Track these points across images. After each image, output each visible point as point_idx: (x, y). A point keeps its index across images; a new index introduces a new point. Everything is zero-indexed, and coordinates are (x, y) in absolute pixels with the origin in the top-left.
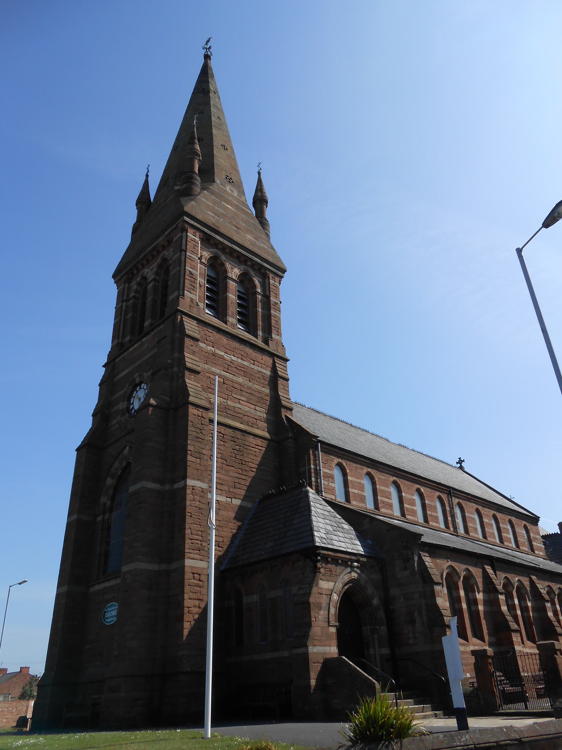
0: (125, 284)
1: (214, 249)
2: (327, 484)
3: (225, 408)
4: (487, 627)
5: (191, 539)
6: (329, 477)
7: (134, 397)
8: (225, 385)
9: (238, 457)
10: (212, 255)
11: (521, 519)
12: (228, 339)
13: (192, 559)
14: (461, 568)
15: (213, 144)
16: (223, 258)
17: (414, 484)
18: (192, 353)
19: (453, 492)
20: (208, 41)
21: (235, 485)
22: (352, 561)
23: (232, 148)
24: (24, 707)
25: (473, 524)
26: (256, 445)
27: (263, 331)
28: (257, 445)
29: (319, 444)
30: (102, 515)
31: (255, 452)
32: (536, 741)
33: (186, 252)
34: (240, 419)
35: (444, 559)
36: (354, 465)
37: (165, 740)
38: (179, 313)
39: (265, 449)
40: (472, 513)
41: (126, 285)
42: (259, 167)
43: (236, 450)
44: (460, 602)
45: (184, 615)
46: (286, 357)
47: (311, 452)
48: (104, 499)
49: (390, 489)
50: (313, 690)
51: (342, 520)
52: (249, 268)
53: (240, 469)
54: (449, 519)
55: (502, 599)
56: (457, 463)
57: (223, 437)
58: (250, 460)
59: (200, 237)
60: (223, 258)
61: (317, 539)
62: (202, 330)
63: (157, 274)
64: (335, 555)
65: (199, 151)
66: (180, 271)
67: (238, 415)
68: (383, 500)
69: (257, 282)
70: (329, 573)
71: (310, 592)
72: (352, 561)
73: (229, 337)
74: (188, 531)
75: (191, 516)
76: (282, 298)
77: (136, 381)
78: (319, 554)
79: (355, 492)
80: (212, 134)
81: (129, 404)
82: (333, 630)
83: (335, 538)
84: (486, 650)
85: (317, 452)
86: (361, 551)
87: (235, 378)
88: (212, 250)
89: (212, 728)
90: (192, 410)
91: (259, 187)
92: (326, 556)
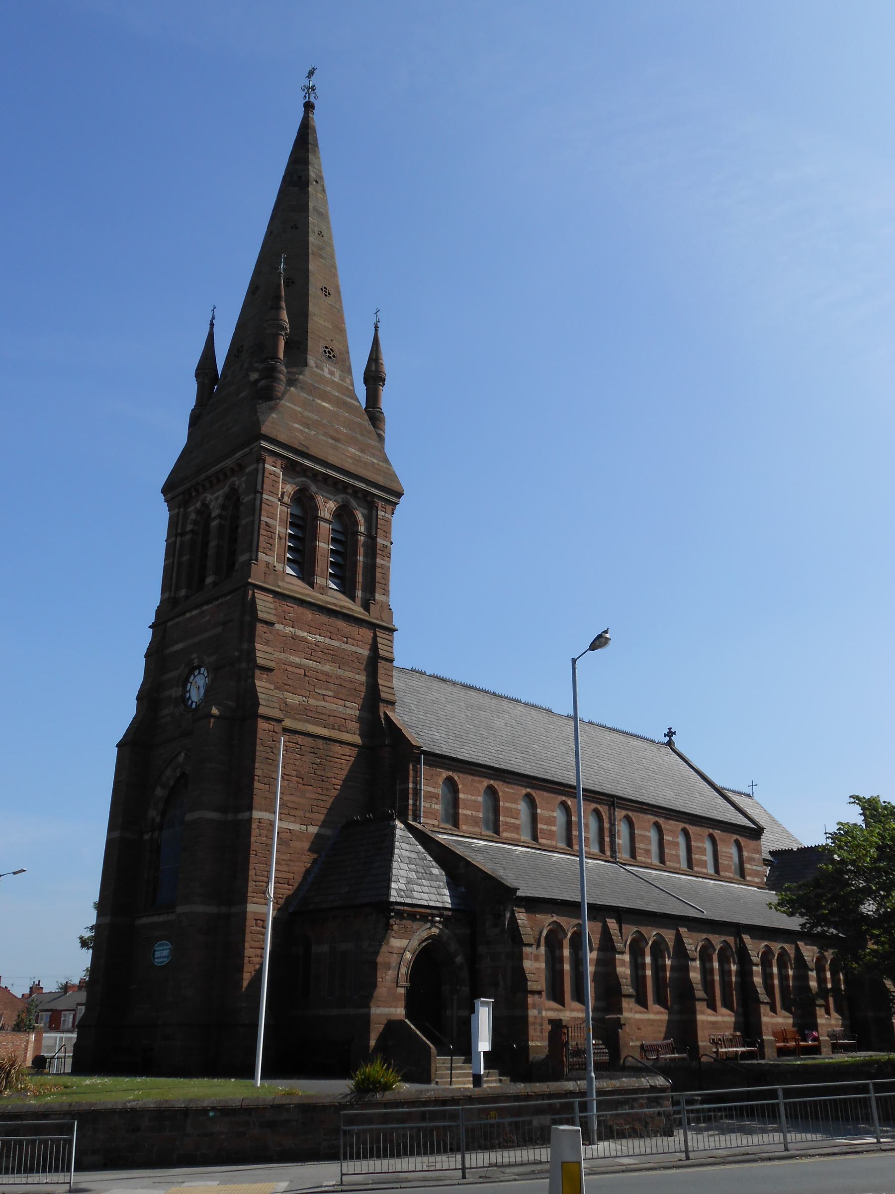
1: (301, 477)
2: (429, 806)
3: (306, 709)
6: (433, 797)
7: (191, 683)
8: (307, 678)
13: (256, 904)
15: (308, 293)
16: (313, 488)
21: (313, 809)
22: (433, 916)
23: (338, 292)
24: (23, 1042)
25: (645, 844)
26: (342, 755)
29: (423, 756)
30: (150, 833)
31: (341, 764)
32: (483, 1097)
33: (262, 493)
34: (324, 722)
36: (470, 778)
37: (220, 1086)
38: (251, 587)
39: (354, 758)
41: (182, 510)
42: (377, 316)
43: (316, 764)
45: (244, 965)
46: (392, 626)
47: (411, 767)
49: (519, 806)
50: (372, 1051)
52: (348, 497)
54: (607, 839)
56: (666, 735)
57: (300, 749)
58: (333, 775)
59: (282, 467)
60: (313, 488)
61: (393, 893)
62: (280, 606)
63: (223, 507)
64: (413, 910)
65: (286, 322)
66: (253, 522)
67: (321, 717)
69: (360, 517)
71: (379, 952)
72: (433, 916)
73: (315, 609)
74: (252, 873)
75: (256, 855)
76: (394, 536)
77: (194, 663)
78: (393, 910)
80: (309, 272)
81: (185, 691)
82: (402, 991)
83: (416, 888)
85: (418, 766)
86: (447, 902)
87: (320, 667)
88: (298, 480)
89: (264, 1081)
90: (262, 725)
91: (374, 354)
92: (402, 912)
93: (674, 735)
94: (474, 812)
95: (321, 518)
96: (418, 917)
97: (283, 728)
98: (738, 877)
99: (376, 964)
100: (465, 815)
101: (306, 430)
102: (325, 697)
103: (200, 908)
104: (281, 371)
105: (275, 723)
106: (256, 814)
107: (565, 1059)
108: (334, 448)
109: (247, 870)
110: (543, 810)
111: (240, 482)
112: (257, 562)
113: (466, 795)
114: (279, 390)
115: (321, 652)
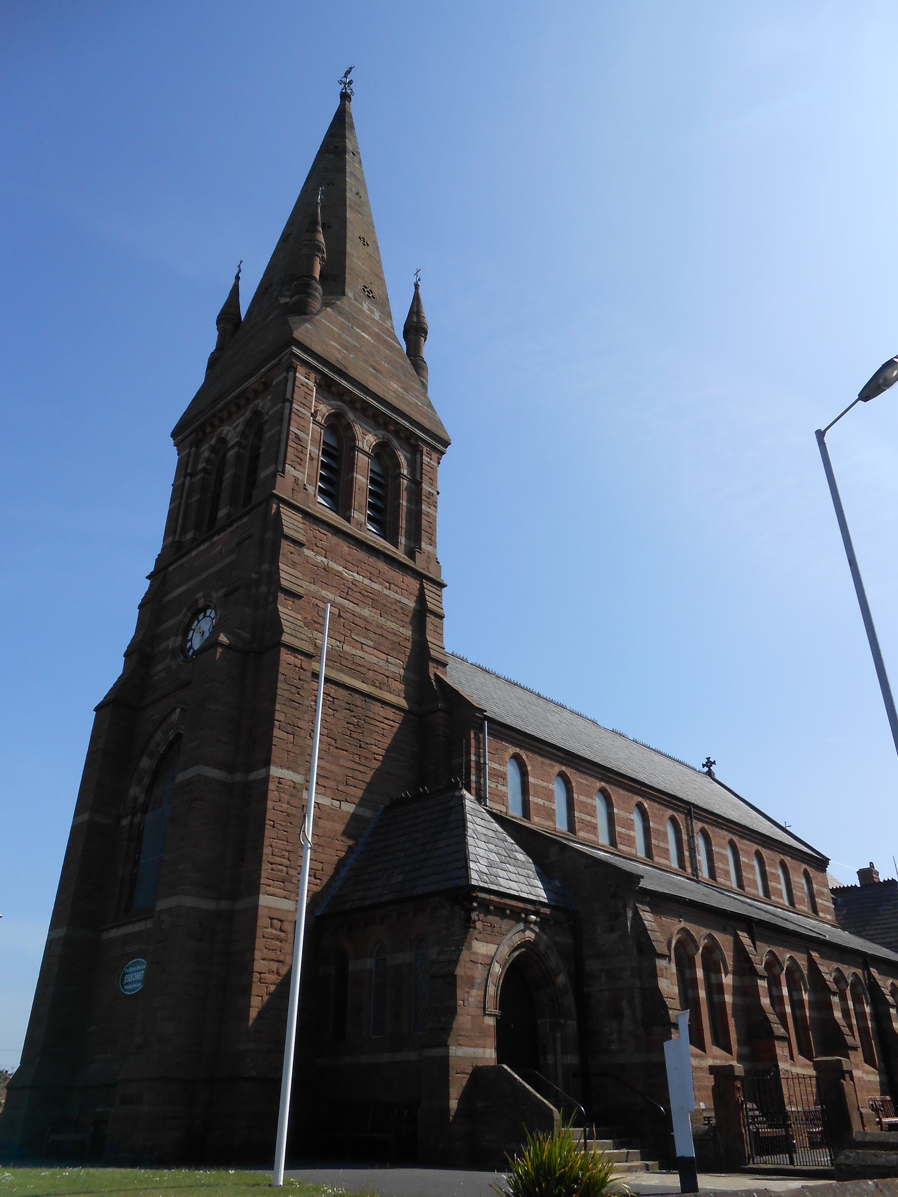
1: (336, 401)
3: (340, 656)
5: (272, 864)
8: (342, 619)
9: (355, 736)
10: (333, 410)
11: (797, 860)
12: (351, 546)
13: (271, 895)
16: (351, 416)
20: (348, 72)
25: (724, 864)
26: (384, 718)
27: (408, 537)
28: (387, 719)
29: (486, 722)
30: (130, 817)
31: (383, 729)
33: (291, 403)
34: (362, 675)
36: (540, 759)
38: (275, 500)
39: (398, 725)
42: (417, 276)
43: (352, 724)
45: (253, 984)
46: (440, 581)
47: (472, 735)
49: (594, 801)
50: (454, 1117)
51: (516, 846)
52: (390, 435)
54: (687, 853)
56: (704, 766)
57: (333, 702)
58: (373, 741)
59: (315, 381)
60: (351, 416)
61: (474, 875)
64: (502, 901)
65: (322, 243)
66: (279, 433)
67: (359, 668)
69: (402, 459)
72: (528, 912)
74: (267, 850)
75: (273, 827)
77: (198, 605)
78: (475, 899)
81: (185, 639)
82: (490, 1021)
84: (733, 1066)
85: (481, 736)
86: (542, 897)
87: (358, 609)
89: (290, 1171)
90: (286, 657)
93: (713, 765)
94: (547, 802)
95: (359, 448)
96: (508, 912)
97: (313, 672)
98: (811, 912)
99: (454, 977)
100: (536, 803)
101: (345, 351)
102: (364, 646)
103: (189, 901)
104: (316, 289)
105: (302, 658)
106: (275, 771)
107: (744, 1131)
108: (376, 378)
109: (261, 846)
110: (620, 809)
111: (263, 403)
112: (284, 475)
113: (536, 779)
114: (314, 306)
115: (360, 593)
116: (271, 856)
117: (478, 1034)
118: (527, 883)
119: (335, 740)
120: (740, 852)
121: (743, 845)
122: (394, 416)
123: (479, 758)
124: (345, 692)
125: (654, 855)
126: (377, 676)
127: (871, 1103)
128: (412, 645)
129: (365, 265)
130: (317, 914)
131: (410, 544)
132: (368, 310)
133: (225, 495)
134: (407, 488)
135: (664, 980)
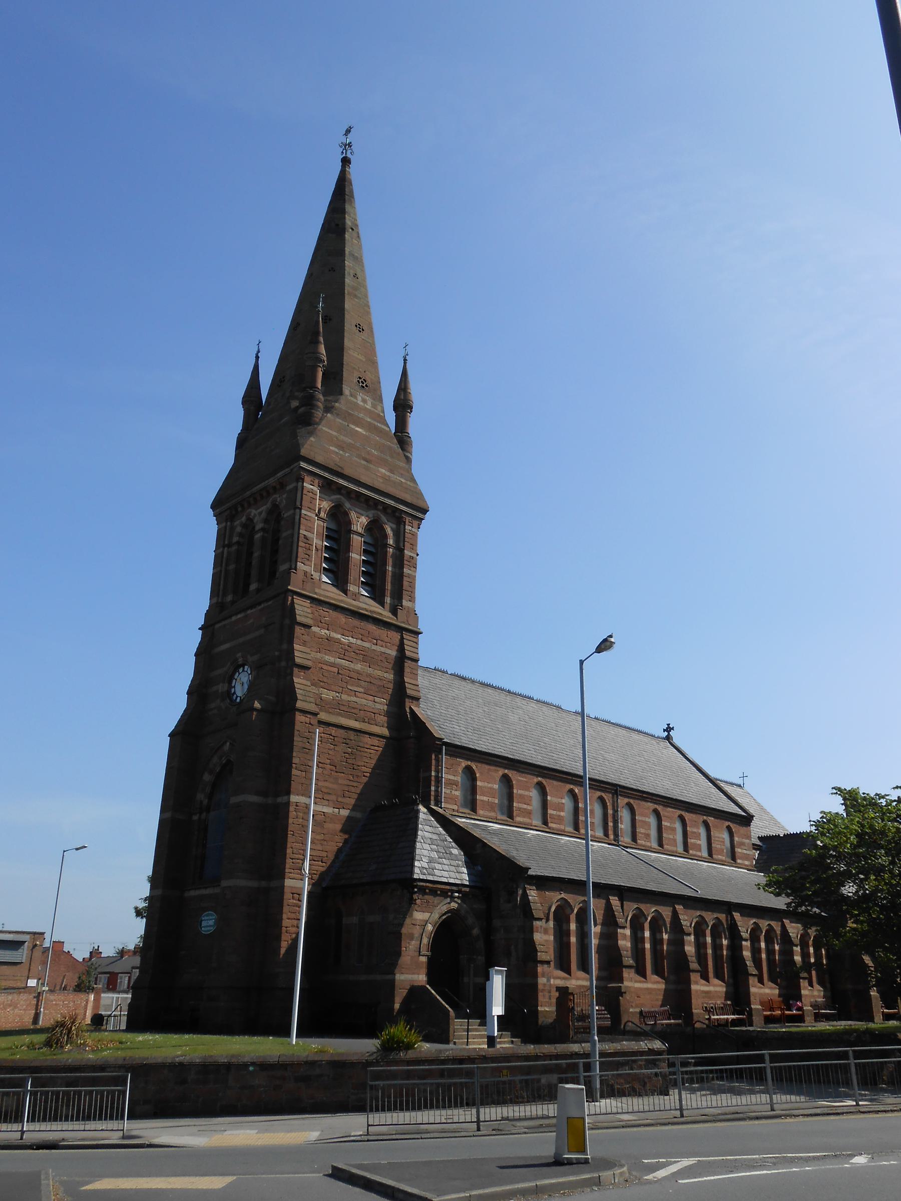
0: (227, 523)
1: (336, 495)
3: (339, 704)
4: (598, 962)
5: (292, 859)
7: (236, 680)
9: (350, 762)
10: (333, 504)
11: (721, 819)
12: (347, 616)
14: (578, 900)
16: (347, 505)
17: (566, 784)
18: (303, 643)
19: (620, 791)
20: (348, 131)
22: (453, 892)
26: (371, 745)
27: (392, 597)
28: (373, 746)
33: (301, 509)
35: (556, 891)
36: (487, 767)
38: (290, 593)
39: (382, 749)
40: (646, 816)
41: (228, 523)
44: (568, 935)
47: (433, 757)
48: (200, 796)
49: (531, 793)
50: (396, 1013)
51: (453, 844)
52: (379, 513)
53: (351, 775)
54: (611, 824)
55: (621, 934)
56: (664, 730)
57: (334, 740)
58: (363, 764)
60: (347, 505)
61: (417, 870)
63: (266, 521)
64: (435, 886)
65: (323, 355)
66: (292, 535)
67: (353, 711)
68: (520, 807)
69: (389, 531)
70: (426, 904)
71: (403, 923)
72: (453, 892)
74: (289, 851)
76: (420, 548)
78: (416, 886)
79: (484, 799)
81: (230, 687)
82: (424, 959)
83: (437, 866)
84: (568, 987)
85: (440, 756)
87: (352, 666)
93: (672, 731)
97: (318, 721)
101: (341, 452)
104: (319, 399)
105: (311, 717)
111: (281, 499)
115: (354, 652)
116: (292, 854)
117: (415, 967)
118: (456, 871)
119: (336, 766)
120: (662, 818)
121: (665, 812)
122: (381, 499)
123: (438, 774)
124: (342, 731)
125: (580, 827)
126: (367, 714)
127: (706, 1005)
128: (394, 686)
129: (361, 354)
130: (324, 886)
131: (394, 602)
132: (362, 402)
133: (254, 572)
134: (393, 555)
135: (539, 934)
